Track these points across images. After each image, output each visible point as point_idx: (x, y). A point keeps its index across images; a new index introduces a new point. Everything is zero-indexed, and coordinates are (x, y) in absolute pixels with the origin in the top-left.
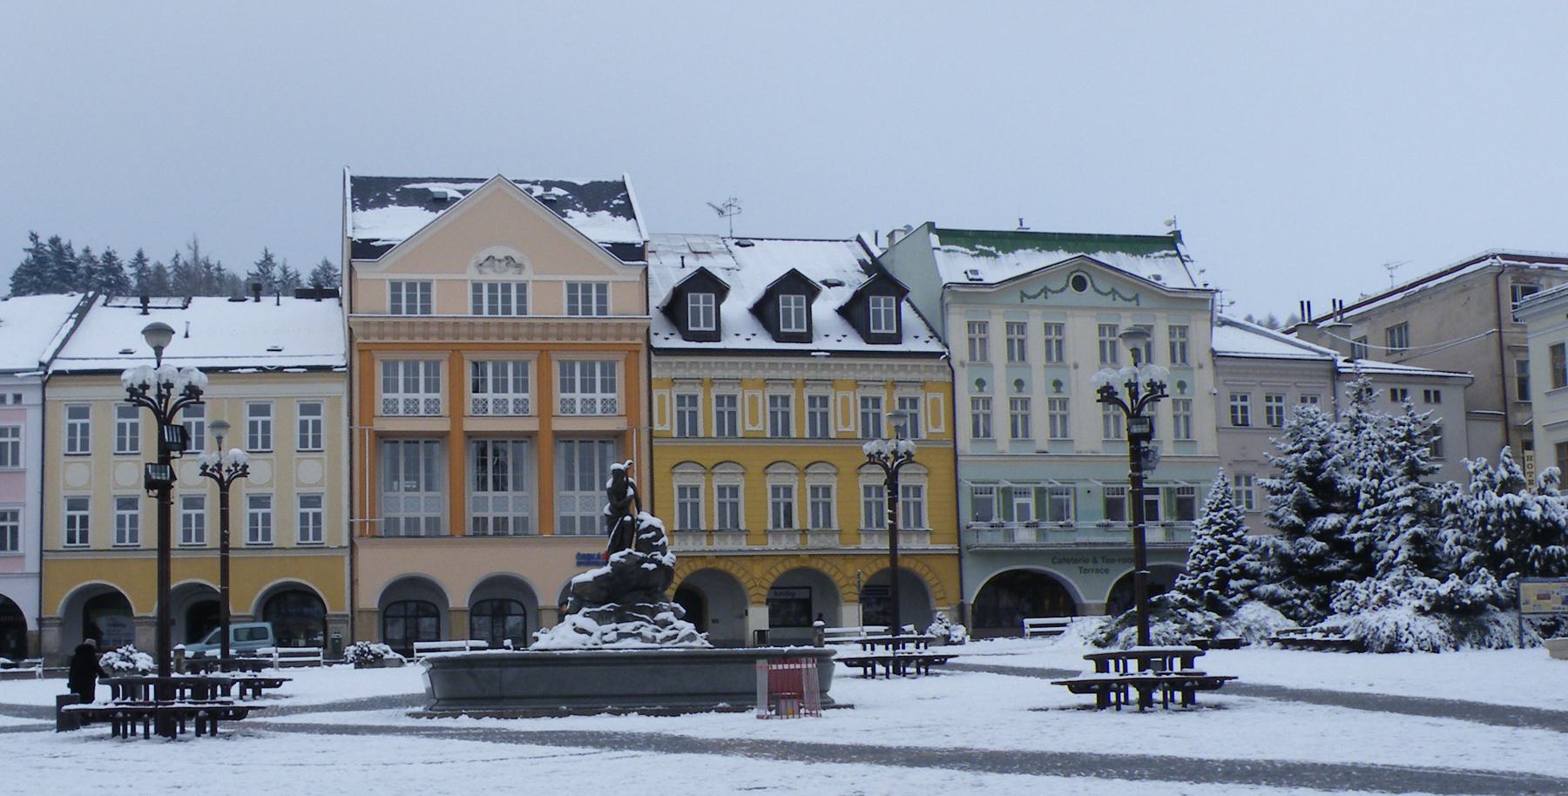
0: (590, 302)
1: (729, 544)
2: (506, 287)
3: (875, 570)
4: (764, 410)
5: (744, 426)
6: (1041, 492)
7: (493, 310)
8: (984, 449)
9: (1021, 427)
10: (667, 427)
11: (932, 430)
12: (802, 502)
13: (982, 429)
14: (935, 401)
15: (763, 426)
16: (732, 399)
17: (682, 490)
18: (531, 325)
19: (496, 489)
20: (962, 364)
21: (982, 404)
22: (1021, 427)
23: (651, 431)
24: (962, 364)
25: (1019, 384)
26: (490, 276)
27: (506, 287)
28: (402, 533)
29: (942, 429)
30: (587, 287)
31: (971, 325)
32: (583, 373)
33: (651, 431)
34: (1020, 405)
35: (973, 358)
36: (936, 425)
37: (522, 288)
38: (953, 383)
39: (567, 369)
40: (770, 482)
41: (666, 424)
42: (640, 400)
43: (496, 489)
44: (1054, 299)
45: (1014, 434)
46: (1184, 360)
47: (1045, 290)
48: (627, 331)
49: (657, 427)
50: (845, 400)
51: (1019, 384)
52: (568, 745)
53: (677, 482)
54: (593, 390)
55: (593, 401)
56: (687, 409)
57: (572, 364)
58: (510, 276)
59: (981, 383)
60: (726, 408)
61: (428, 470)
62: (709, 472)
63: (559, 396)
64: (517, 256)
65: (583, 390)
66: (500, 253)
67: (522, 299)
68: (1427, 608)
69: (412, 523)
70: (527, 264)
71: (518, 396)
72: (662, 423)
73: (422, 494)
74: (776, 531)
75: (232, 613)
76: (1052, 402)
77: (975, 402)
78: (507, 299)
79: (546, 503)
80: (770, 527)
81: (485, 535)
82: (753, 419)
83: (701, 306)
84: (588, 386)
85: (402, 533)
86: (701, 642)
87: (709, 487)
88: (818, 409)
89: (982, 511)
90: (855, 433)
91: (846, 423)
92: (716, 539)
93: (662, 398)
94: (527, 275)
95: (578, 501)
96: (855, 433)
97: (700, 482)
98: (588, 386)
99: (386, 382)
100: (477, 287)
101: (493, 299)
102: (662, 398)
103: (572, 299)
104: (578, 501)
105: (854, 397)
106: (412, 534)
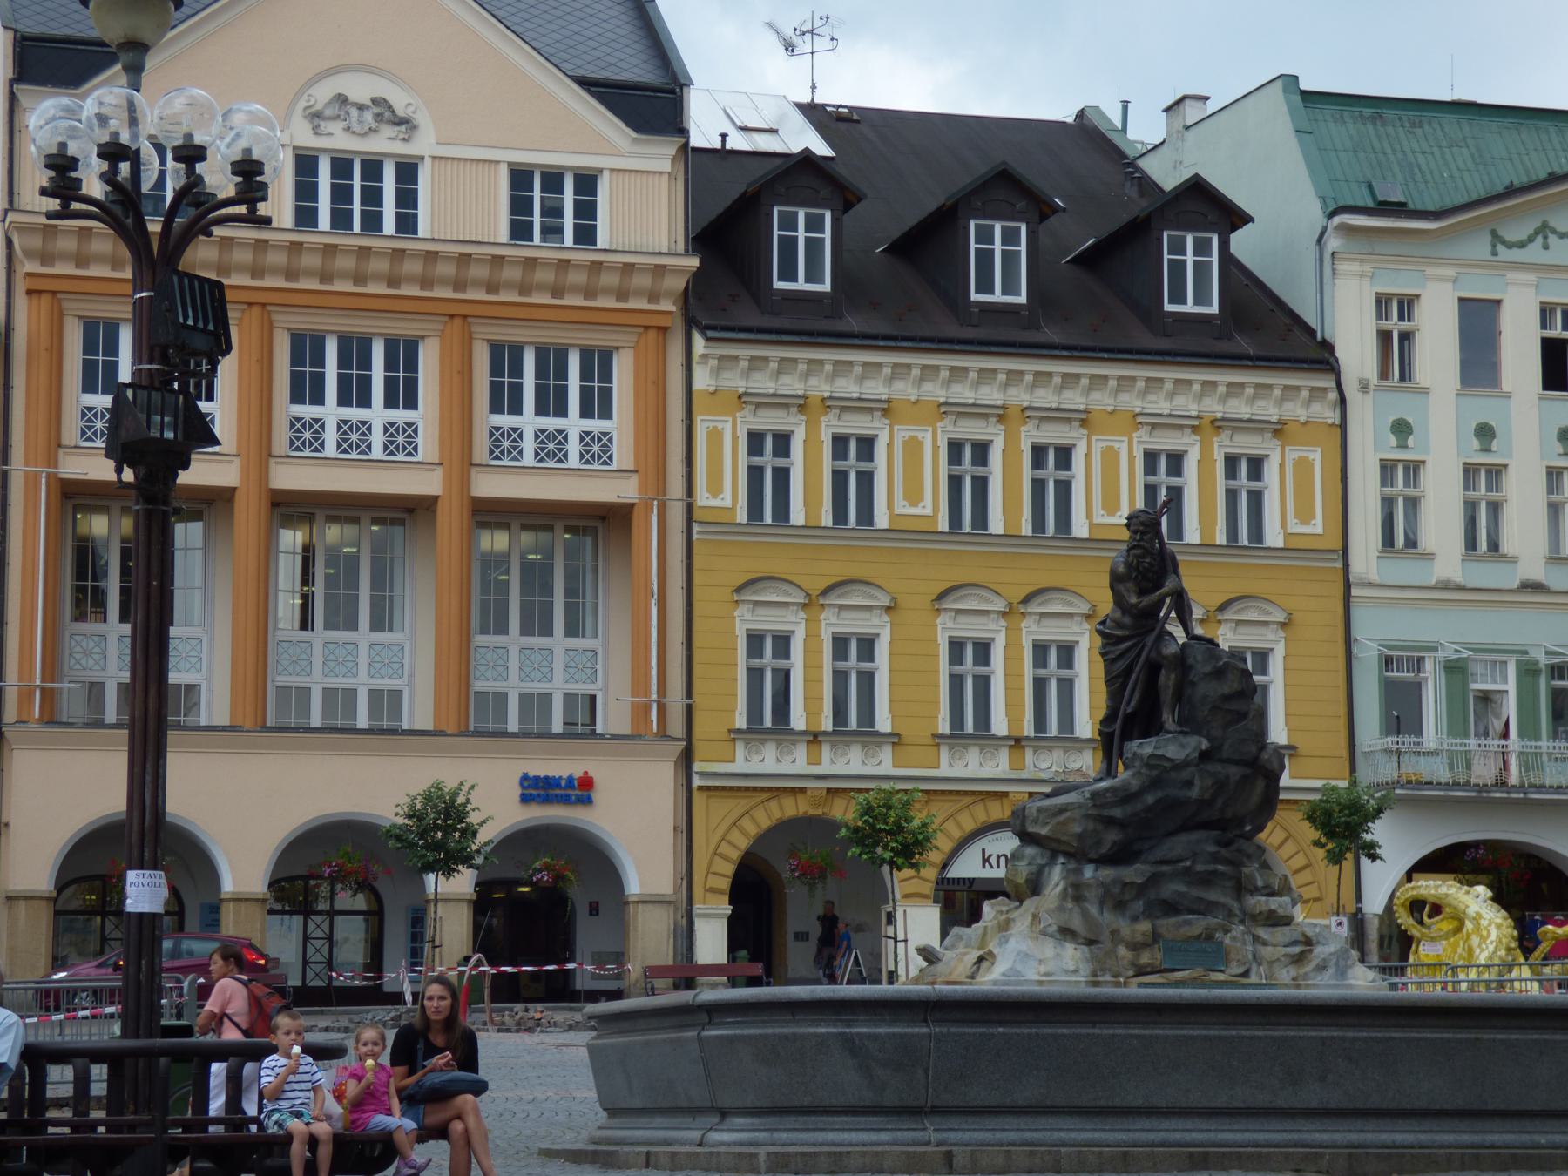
0: (314, 196)
1: (851, 762)
2: (373, 169)
3: (766, 823)
4: (934, 470)
6: (1528, 672)
7: (341, 220)
8: (1403, 571)
9: (1482, 533)
11: (1295, 527)
12: (811, 667)
13: (1399, 536)
14: (1303, 466)
15: (932, 506)
16: (867, 446)
17: (956, 647)
18: (431, 257)
19: (526, 630)
20: (1364, 387)
21: (1402, 473)
22: (1482, 533)
23: (689, 508)
24: (1364, 387)
25: (1485, 433)
26: (338, 139)
27: (373, 169)
28: (513, 725)
29: (1317, 527)
31: (1382, 302)
32: (541, 372)
33: (689, 508)
34: (1483, 476)
35: (1384, 373)
36: (1305, 515)
37: (407, 171)
39: (306, 348)
40: (945, 629)
41: (724, 493)
42: (667, 440)
43: (526, 630)
45: (1471, 544)
46: (1402, 378)
48: (642, 281)
49: (702, 498)
50: (1110, 457)
51: (1485, 433)
53: (744, 621)
56: (768, 460)
57: (562, 354)
58: (384, 143)
59: (1402, 429)
60: (1050, 472)
61: (571, 592)
62: (811, 605)
63: (486, 420)
64: (400, 101)
66: (360, 89)
67: (407, 199)
69: (535, 705)
70: (422, 118)
72: (716, 489)
73: (559, 640)
74: (956, 738)
76: (1470, 471)
77: (1387, 468)
78: (373, 196)
79: (457, 664)
80: (944, 728)
81: (99, 724)
82: (910, 490)
83: (801, 234)
85: (513, 725)
86: (1526, 985)
87: (812, 637)
88: (1050, 472)
89: (1402, 713)
90: (933, 518)
91: (914, 496)
92: (826, 751)
94: (422, 145)
95: (559, 653)
96: (933, 518)
97: (883, 630)
101: (341, 194)
102: (715, 437)
103: (520, 206)
104: (559, 653)
105: (933, 441)
106: (340, 731)
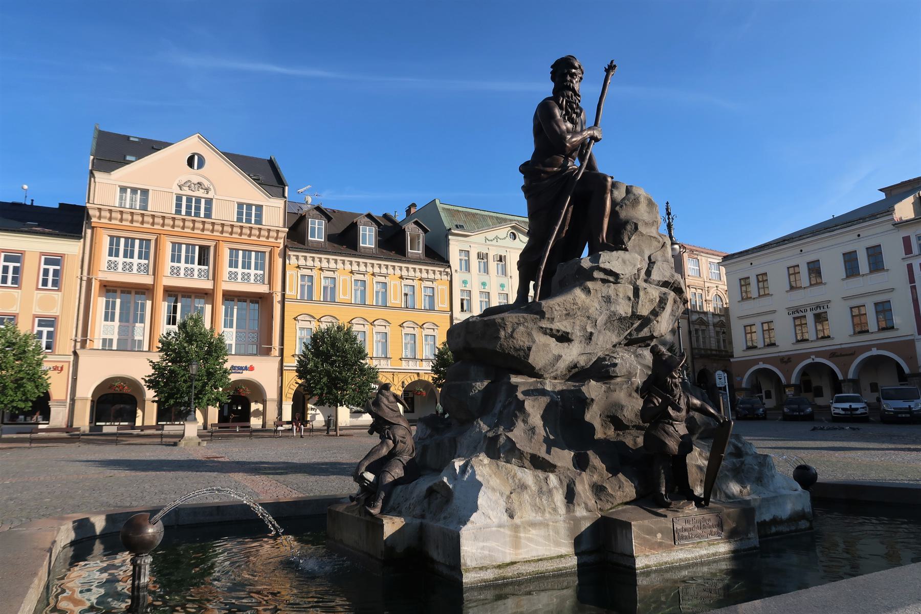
5: (340, 296)
10: (294, 293)
23: (283, 296)
26: (186, 191)
27: (198, 201)
30: (249, 206)
38: (451, 282)
44: (500, 243)
47: (497, 238)
52: (185, 470)
54: (179, 261)
55: (192, 270)
58: (200, 193)
65: (243, 267)
68: (593, 389)
71: (187, 265)
75: (576, 578)
84: (129, 254)
93: (291, 276)
98: (129, 254)
99: (231, 261)
100: (179, 198)
101: (189, 207)
